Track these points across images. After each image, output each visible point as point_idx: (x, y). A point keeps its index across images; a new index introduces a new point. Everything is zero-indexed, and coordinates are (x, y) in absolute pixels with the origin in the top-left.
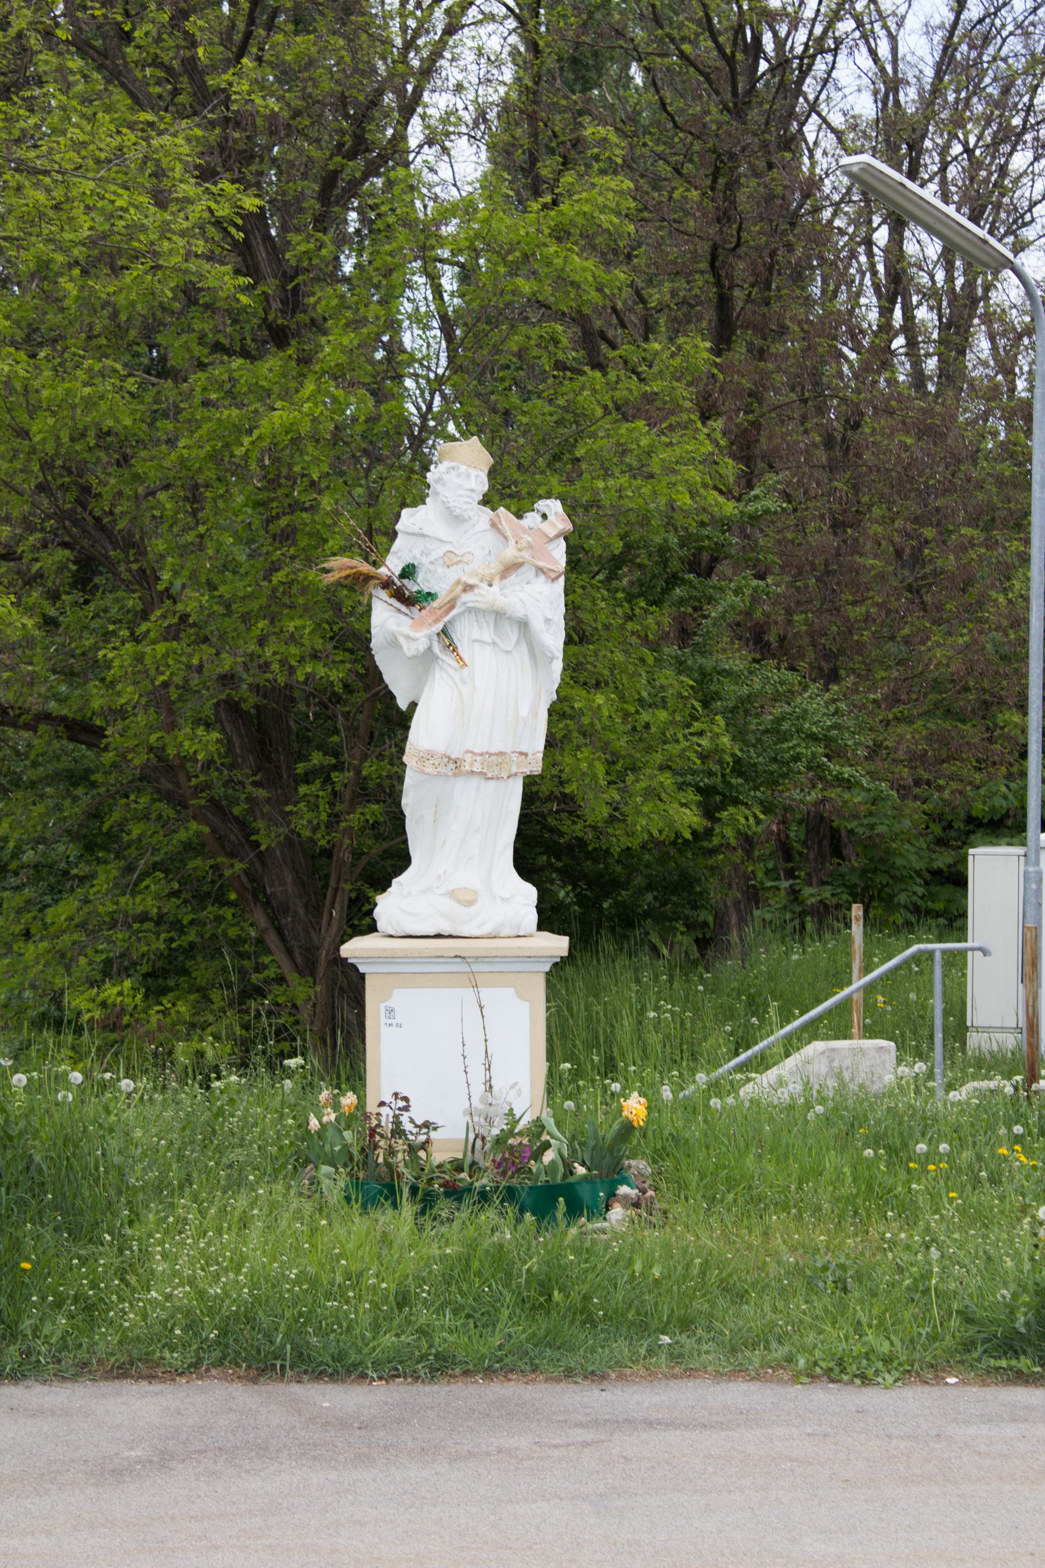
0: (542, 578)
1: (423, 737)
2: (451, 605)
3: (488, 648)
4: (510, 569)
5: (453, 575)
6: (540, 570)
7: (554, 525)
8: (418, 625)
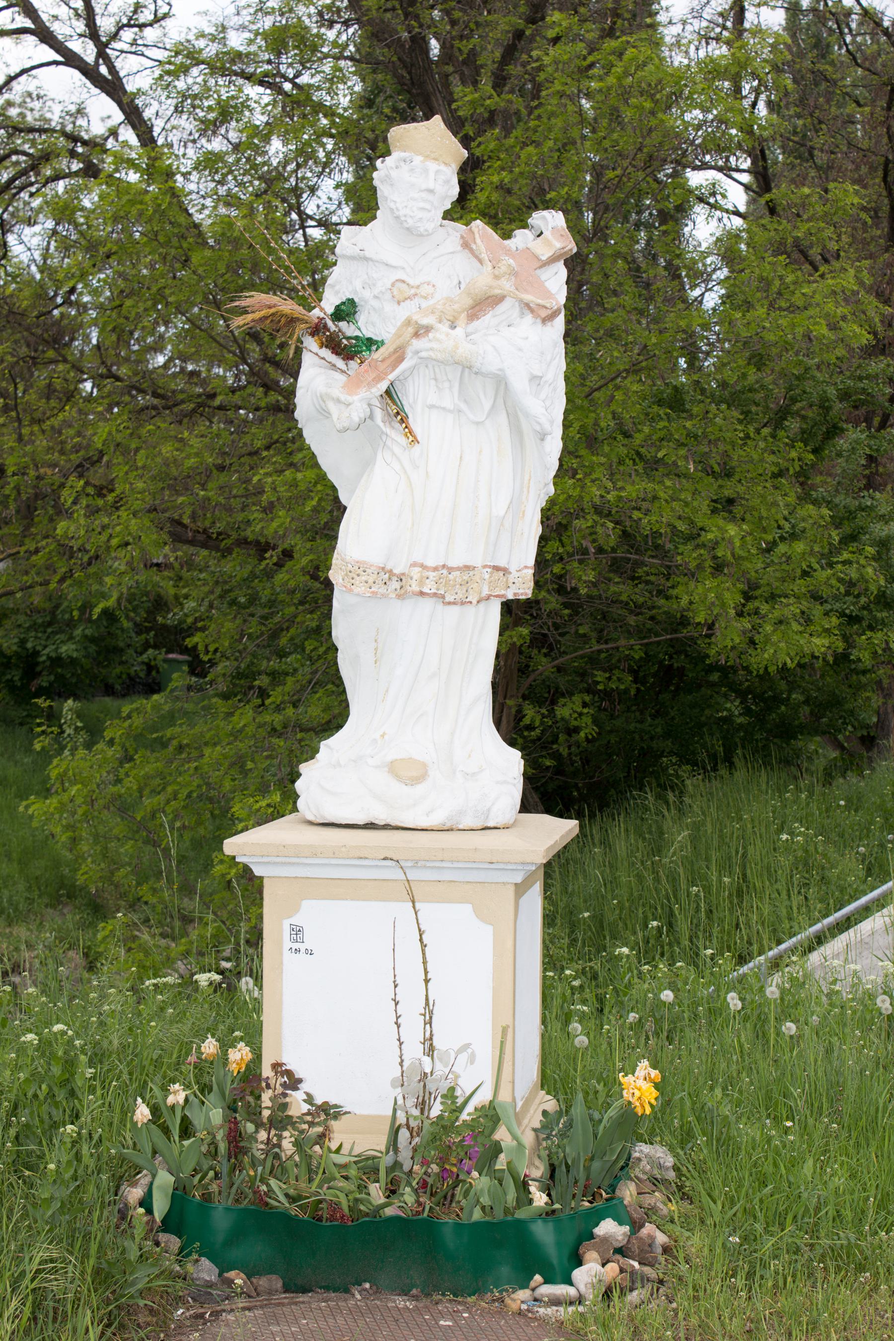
0: (529, 318)
1: (358, 544)
2: (399, 356)
4: (482, 304)
5: (407, 310)
7: (548, 243)
8: (353, 384)
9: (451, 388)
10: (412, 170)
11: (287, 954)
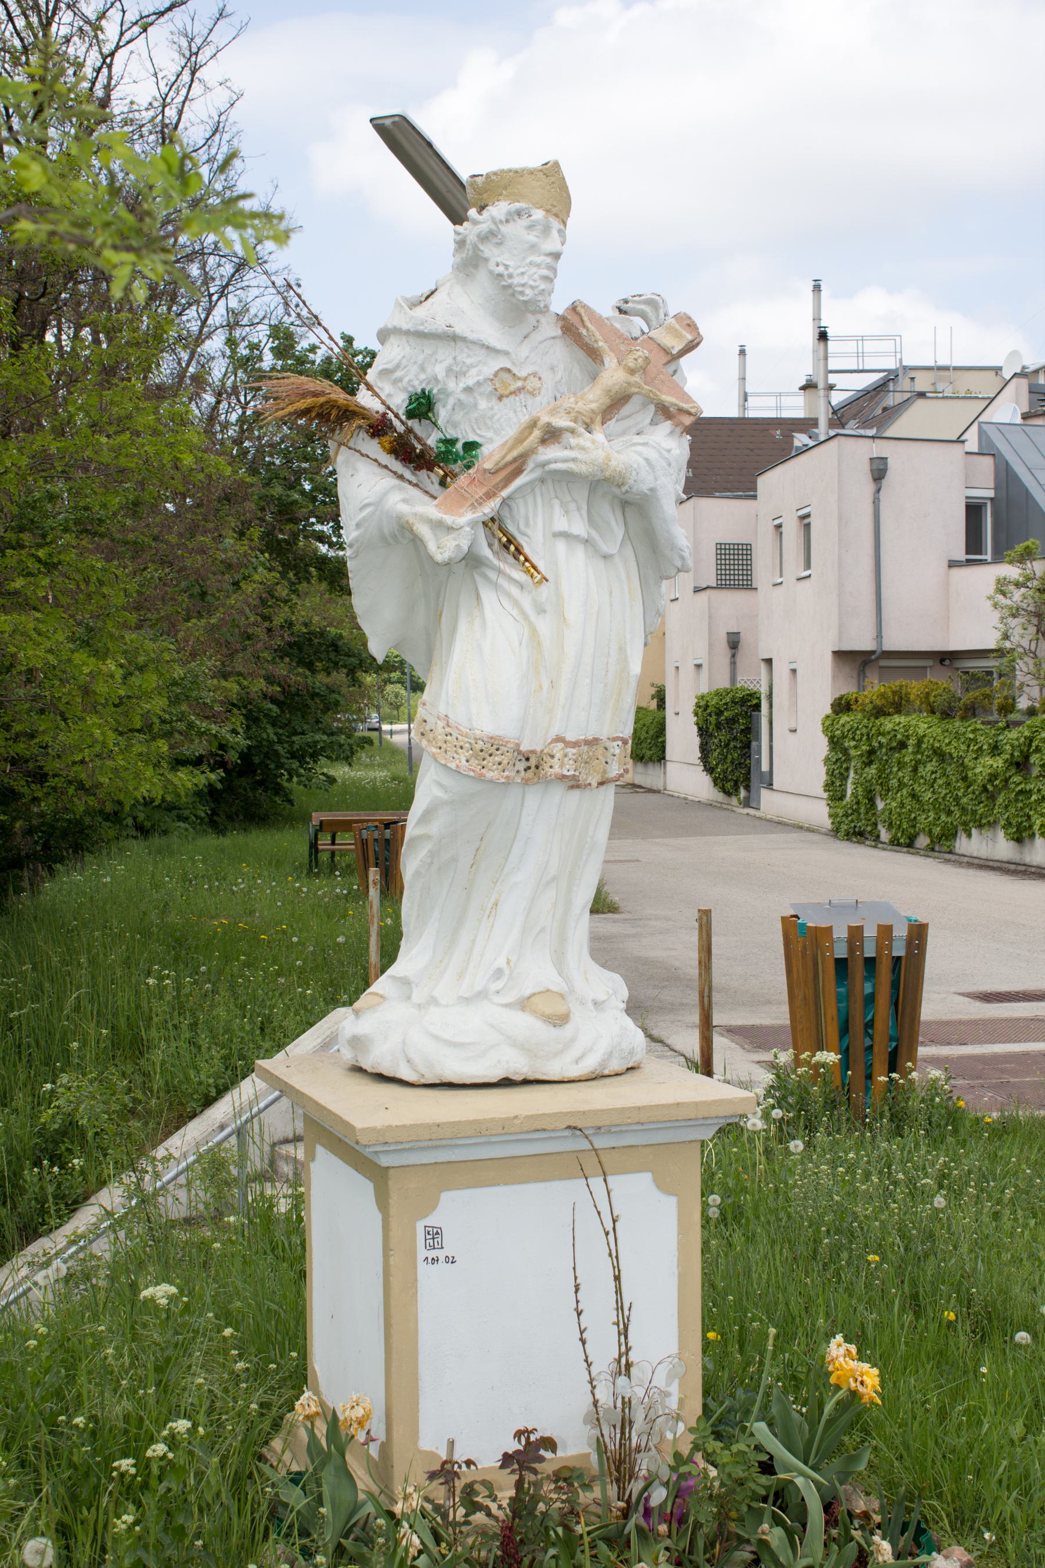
3: (580, 552)
10: (530, 227)
11: (421, 1266)
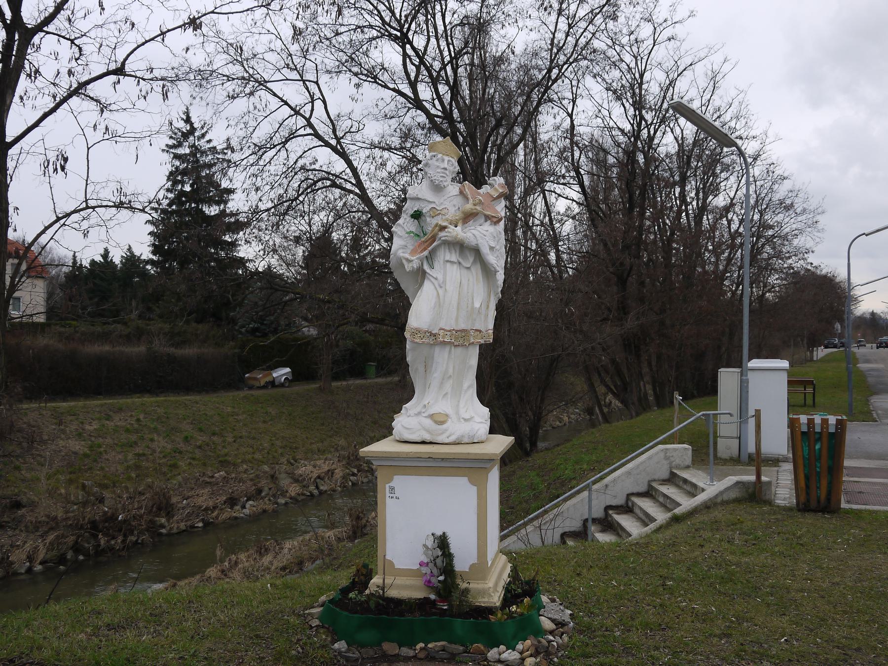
6: (487, 218)
7: (496, 190)
9: (802, 341)
10: (437, 160)
11: (387, 498)
